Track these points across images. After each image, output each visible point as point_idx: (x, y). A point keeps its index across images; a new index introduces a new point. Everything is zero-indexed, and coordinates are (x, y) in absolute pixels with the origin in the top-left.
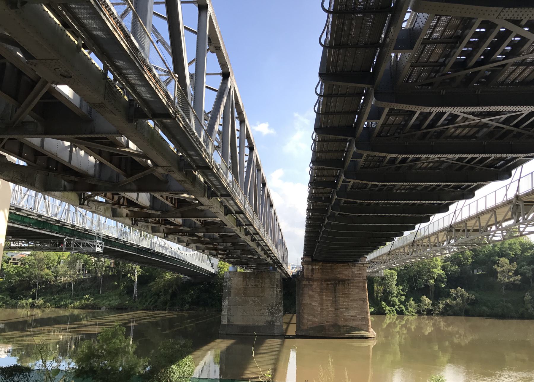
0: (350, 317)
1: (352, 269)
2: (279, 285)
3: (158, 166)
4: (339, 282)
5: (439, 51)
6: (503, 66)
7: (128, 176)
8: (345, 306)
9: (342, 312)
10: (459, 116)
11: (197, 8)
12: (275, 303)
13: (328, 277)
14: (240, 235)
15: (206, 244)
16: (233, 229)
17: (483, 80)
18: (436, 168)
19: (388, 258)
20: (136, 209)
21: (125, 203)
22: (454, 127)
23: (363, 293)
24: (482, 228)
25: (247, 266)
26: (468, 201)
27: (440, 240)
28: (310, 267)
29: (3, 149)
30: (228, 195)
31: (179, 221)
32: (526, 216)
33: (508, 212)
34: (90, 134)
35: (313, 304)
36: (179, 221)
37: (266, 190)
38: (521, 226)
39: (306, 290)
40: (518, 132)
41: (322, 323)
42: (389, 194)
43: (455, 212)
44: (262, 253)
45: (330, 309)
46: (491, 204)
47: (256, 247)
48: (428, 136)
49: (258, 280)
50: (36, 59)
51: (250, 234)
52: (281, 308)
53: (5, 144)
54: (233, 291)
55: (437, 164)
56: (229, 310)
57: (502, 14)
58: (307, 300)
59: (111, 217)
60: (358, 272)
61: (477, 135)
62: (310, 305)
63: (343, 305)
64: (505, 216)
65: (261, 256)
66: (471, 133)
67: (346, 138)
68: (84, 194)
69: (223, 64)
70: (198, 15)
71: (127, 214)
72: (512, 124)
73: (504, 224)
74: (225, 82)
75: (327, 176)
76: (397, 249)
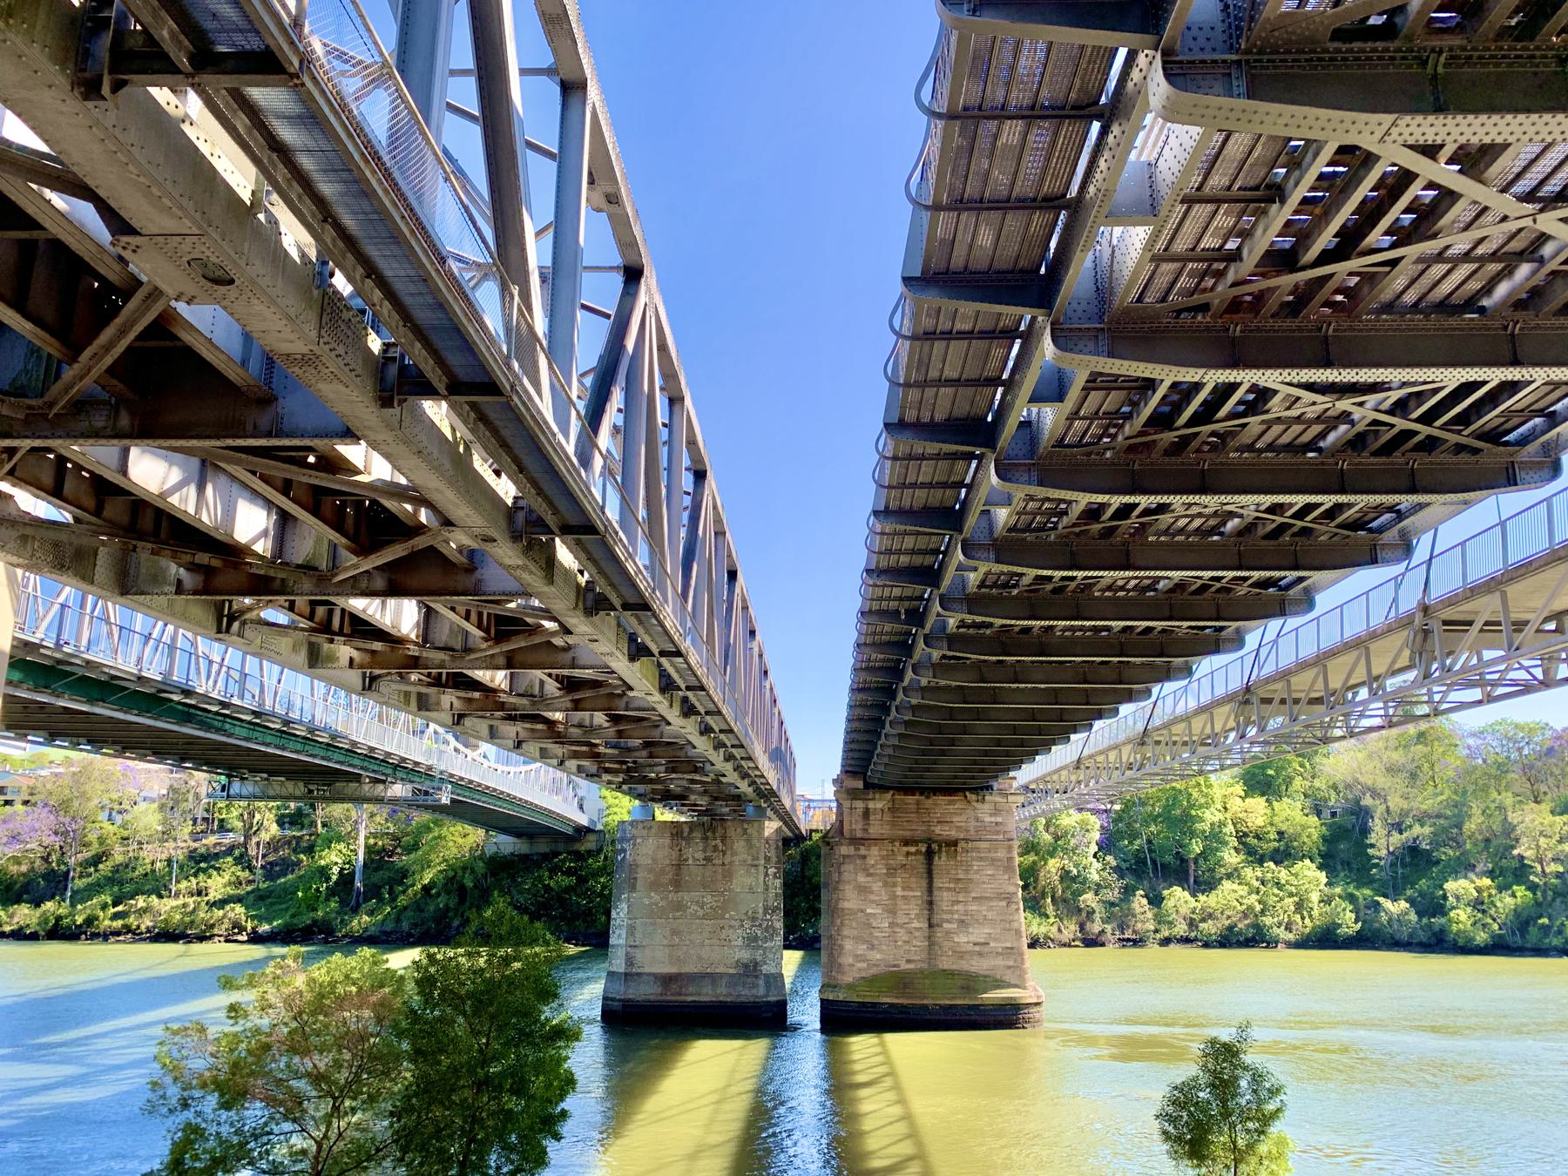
0: (970, 947)
1: (975, 809)
2: (774, 859)
3: (453, 525)
4: (940, 846)
5: (1224, 220)
6: (1394, 263)
7: (362, 550)
8: (956, 916)
9: (948, 933)
10: (1275, 392)
11: (557, 90)
12: (761, 911)
13: (908, 833)
14: (669, 718)
15: (572, 743)
16: (649, 698)
17: (1339, 298)
18: (1213, 531)
19: (1073, 778)
20: (377, 646)
21: (347, 630)
22: (1263, 422)
23: (1006, 877)
24: (1333, 695)
25: (683, 805)
26: (1293, 622)
27: (1218, 728)
28: (859, 804)
29: (11, 475)
30: (641, 606)
31: (498, 678)
32: (1448, 662)
33: (1400, 651)
34: (269, 435)
35: (869, 911)
36: (498, 678)
37: (738, 590)
38: (1436, 689)
39: (848, 868)
40: (1429, 437)
41: (894, 966)
42: (1077, 603)
43: (1258, 650)
44: (728, 767)
45: (916, 924)
46: (1355, 627)
47: (711, 751)
48: (1195, 444)
49: (714, 843)
50: (140, 234)
51: (698, 713)
52: (779, 925)
53: (16, 464)
54: (641, 875)
55: (1212, 522)
56: (631, 930)
57: (1394, 131)
58: (850, 900)
59: (306, 666)
60: (993, 819)
61: (1322, 444)
62: (860, 914)
63: (951, 912)
64: (1393, 662)
65: (724, 775)
66: (1306, 438)
67: (970, 449)
68: (230, 602)
69: (627, 243)
70: (559, 107)
71: (351, 660)
72: (1415, 415)
73: (1391, 684)
74: (631, 291)
75: (912, 552)
76: (1101, 753)
